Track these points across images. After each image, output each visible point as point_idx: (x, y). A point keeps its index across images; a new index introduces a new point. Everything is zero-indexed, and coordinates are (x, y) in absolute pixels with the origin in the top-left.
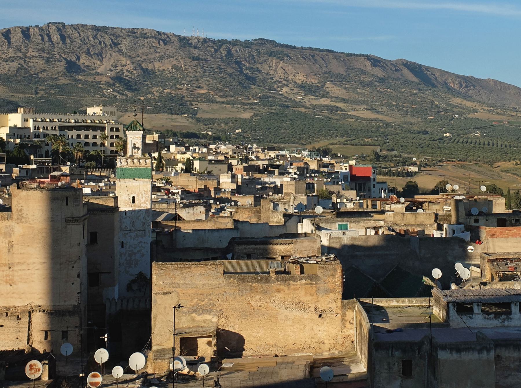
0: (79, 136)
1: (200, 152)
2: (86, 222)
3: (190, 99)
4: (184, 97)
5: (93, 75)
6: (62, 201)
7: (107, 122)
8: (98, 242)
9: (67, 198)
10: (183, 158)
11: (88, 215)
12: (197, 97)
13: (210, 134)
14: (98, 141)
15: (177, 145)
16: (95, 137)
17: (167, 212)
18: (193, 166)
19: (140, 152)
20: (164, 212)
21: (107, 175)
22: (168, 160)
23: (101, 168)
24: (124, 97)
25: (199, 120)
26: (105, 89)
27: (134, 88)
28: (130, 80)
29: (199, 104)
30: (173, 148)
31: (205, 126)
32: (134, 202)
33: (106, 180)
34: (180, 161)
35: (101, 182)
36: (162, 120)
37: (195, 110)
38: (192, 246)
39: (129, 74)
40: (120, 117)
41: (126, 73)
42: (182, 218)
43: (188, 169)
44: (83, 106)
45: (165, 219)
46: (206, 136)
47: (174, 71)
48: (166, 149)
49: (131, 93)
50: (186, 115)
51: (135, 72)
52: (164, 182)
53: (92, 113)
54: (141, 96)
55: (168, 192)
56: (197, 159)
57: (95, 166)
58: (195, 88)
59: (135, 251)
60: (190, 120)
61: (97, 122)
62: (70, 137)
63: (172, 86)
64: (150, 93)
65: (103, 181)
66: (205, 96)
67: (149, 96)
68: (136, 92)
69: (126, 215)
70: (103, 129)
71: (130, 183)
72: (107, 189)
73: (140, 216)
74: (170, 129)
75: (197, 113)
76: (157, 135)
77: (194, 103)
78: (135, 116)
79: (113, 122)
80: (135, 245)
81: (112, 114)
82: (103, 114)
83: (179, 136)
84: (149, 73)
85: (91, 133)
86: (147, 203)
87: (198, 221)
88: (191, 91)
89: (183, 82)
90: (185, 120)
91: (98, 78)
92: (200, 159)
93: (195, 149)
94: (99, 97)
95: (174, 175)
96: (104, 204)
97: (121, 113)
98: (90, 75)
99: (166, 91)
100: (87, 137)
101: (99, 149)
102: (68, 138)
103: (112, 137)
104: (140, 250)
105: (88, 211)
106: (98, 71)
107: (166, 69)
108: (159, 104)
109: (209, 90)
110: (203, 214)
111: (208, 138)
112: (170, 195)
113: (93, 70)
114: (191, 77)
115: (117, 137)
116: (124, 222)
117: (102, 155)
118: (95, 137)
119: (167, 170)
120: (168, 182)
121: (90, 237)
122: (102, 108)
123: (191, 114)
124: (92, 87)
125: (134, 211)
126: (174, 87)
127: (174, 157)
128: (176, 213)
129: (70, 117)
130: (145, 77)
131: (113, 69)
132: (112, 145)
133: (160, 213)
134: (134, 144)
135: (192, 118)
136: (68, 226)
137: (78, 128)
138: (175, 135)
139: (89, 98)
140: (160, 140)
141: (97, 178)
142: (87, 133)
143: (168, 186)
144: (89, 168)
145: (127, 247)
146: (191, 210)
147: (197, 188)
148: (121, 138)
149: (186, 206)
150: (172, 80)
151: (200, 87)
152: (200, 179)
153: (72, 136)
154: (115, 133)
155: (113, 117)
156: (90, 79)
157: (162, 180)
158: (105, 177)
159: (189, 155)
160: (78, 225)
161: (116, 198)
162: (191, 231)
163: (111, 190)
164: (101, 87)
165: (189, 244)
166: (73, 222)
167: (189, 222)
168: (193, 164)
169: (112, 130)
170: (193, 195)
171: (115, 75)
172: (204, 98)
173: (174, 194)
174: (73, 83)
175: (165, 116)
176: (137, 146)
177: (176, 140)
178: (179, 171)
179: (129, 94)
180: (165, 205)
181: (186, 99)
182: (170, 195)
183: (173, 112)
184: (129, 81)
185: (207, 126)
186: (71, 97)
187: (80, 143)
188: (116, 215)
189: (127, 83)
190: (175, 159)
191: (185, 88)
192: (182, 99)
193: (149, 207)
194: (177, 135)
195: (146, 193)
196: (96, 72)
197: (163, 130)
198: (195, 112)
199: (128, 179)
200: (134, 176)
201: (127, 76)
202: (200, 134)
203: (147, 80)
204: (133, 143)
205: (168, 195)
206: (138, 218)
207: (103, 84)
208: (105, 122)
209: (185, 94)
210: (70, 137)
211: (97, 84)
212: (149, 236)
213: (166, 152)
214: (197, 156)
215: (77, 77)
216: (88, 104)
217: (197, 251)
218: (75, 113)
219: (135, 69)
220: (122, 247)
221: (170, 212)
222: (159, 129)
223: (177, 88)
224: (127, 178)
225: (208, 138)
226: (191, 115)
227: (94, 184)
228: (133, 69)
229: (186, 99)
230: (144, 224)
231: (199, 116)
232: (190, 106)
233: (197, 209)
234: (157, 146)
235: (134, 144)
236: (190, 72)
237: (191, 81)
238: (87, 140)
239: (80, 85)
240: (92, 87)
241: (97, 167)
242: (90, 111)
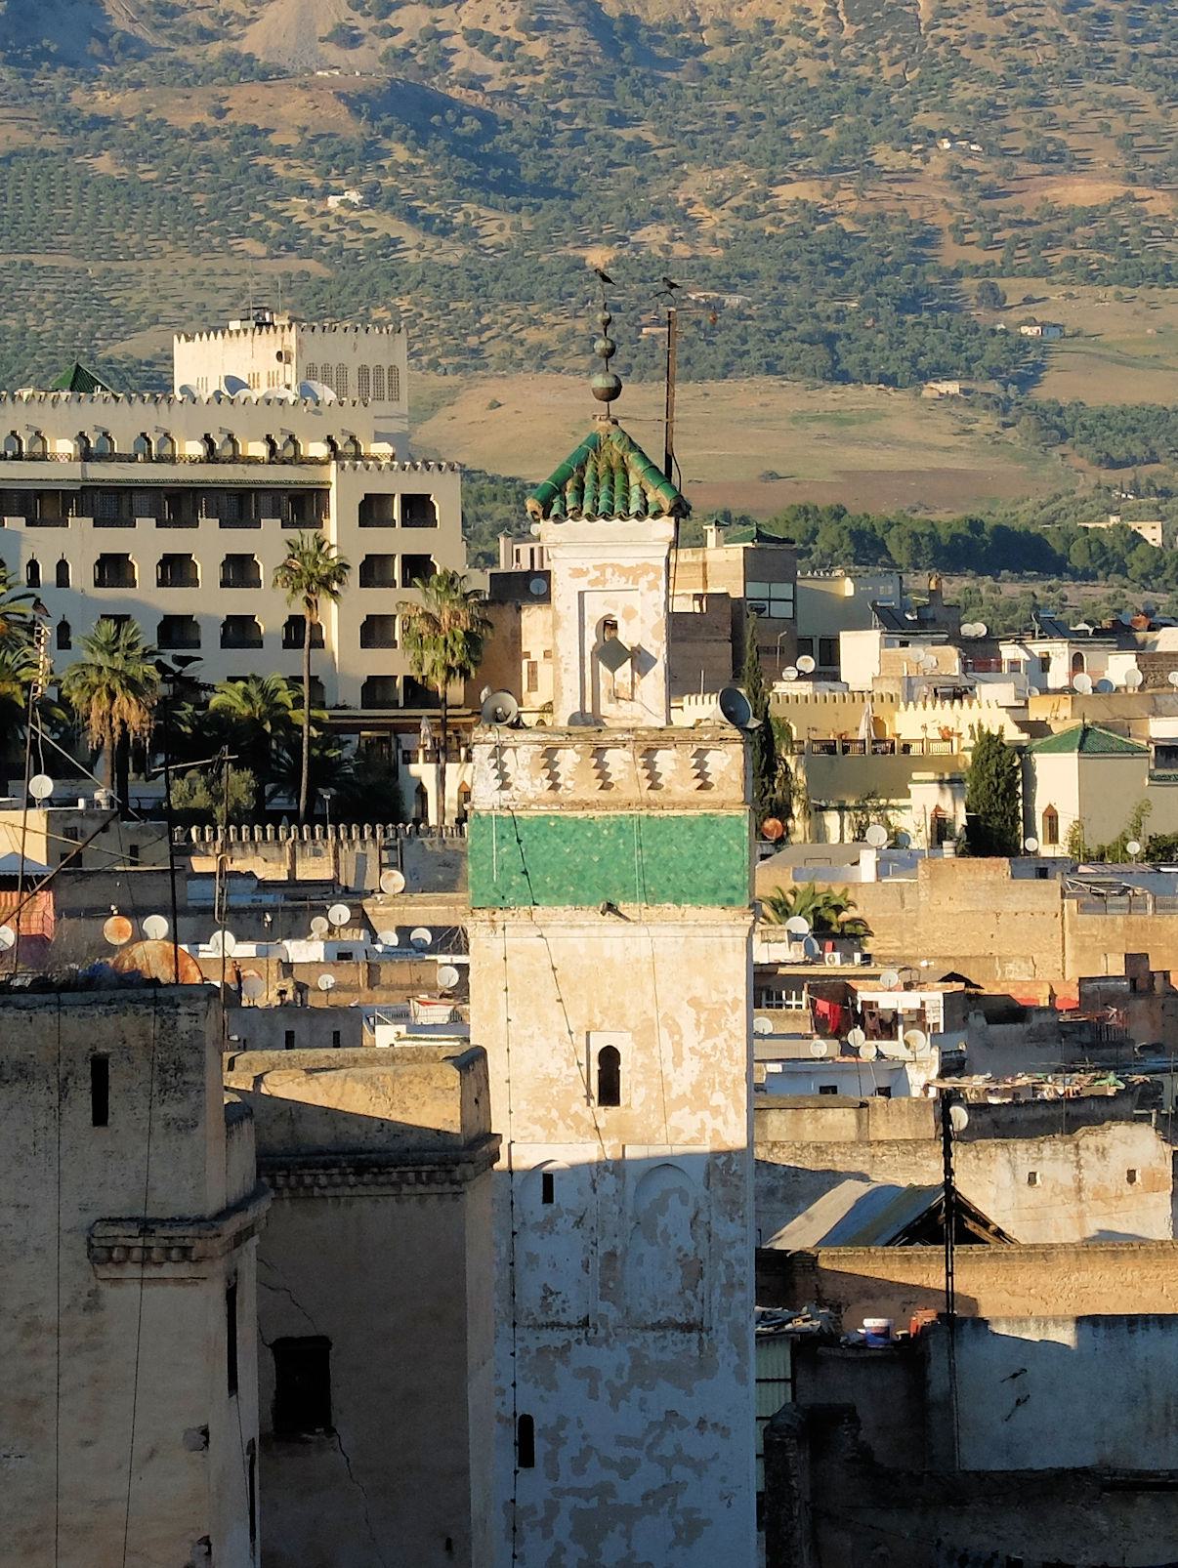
0: (113, 569)
1: (1084, 682)
2: (248, 1261)
3: (977, 256)
4: (929, 238)
5: (202, 76)
6: (63, 1090)
7: (335, 453)
8: (337, 1419)
9: (100, 1068)
10: (947, 736)
11: (265, 1205)
12: (1041, 243)
13: (1152, 533)
14: (269, 606)
15: (901, 624)
16: (239, 570)
17: (863, 1177)
18: (1029, 798)
19: (654, 683)
20: (831, 1179)
21: (348, 879)
22: (829, 748)
23: (294, 817)
24: (454, 253)
25: (1057, 427)
26: (304, 189)
27: (529, 174)
28: (502, 110)
29: (1056, 295)
30: (862, 653)
31: (1108, 476)
32: (609, 1093)
33: (341, 913)
34: (925, 762)
35: (303, 933)
36: (752, 429)
37: (1023, 344)
38: (1086, 1457)
39: (492, 67)
40: (425, 410)
41: (466, 59)
42: (985, 1223)
43: (994, 826)
44: (127, 323)
45: (850, 1232)
46: (1112, 558)
47: (848, 32)
48: (807, 663)
49: (508, 219)
50: (952, 387)
51: (538, 49)
52: (801, 925)
53: (216, 384)
54: (585, 243)
55: (841, 1012)
56: (1060, 745)
57: (247, 801)
58: (1024, 168)
59: (629, 1492)
60: (987, 422)
61: (259, 450)
62: (47, 574)
63: (839, 151)
64: (657, 216)
65: (319, 924)
66: (1102, 226)
67: (653, 236)
68: (552, 208)
69: (548, 1197)
70: (303, 505)
71: (575, 936)
72: (353, 989)
73: (661, 1206)
74: (825, 500)
75: (1039, 367)
76: (735, 553)
77: (1013, 288)
78: (613, 393)
79: (384, 449)
80: (622, 1441)
81: (376, 383)
82: (305, 391)
83: (900, 555)
84: (644, 57)
85: (208, 542)
86: (718, 1099)
87: (1111, 1245)
88: (989, 193)
89: (924, 119)
90: (947, 423)
91: (247, 103)
92: (1084, 741)
93: (1045, 663)
94: (258, 249)
95: (882, 871)
96: (380, 1110)
97: (435, 380)
98: (188, 77)
99: (786, 193)
100: (176, 570)
101: (274, 665)
102: (34, 580)
103: (374, 571)
104: (671, 1489)
105: (261, 1168)
106: (245, 47)
107: (784, 19)
108: (733, 300)
109: (1132, 179)
110: (1153, 1187)
111: (1137, 568)
112: (856, 1036)
113: (206, 36)
114: (987, 77)
115: (418, 567)
116: (533, 1259)
117: (299, 716)
118: (239, 570)
119: (819, 834)
120: (832, 928)
121: (272, 1375)
122: (291, 340)
123: (993, 373)
124: (203, 176)
125: (616, 1168)
126: (849, 163)
127: (877, 723)
128: (948, 1187)
129: (42, 416)
130: (621, 87)
131: (363, 24)
132: (375, 632)
133: (795, 1188)
134: (608, 625)
135: (1003, 406)
136: (110, 1293)
137: (110, 504)
138: (866, 547)
139: (172, 267)
140: (759, 590)
141: (268, 900)
142: (176, 540)
143: (834, 963)
144: (203, 818)
145: (564, 1456)
146: (1051, 1160)
147: (1073, 974)
148: (451, 581)
149: (1003, 1123)
150: (838, 106)
151: (1057, 159)
152: (1097, 899)
153: (62, 566)
154: (398, 541)
155: (384, 407)
156: (187, 113)
157: (783, 910)
158: (331, 890)
159: (991, 708)
160: (196, 1280)
161: (471, 1062)
162: (1065, 1336)
163: (381, 997)
164: (267, 177)
165: (1058, 1442)
166: (144, 1262)
167: (1042, 1253)
168: (1030, 781)
169: (372, 510)
170: (1038, 1038)
171: (383, 76)
172: (1100, 243)
173: (887, 1026)
174: (50, 142)
175: (788, 397)
176: (627, 637)
177: (887, 591)
178: (919, 842)
179: (497, 227)
180: (839, 1121)
181: (950, 254)
182: (856, 1036)
183: (850, 362)
184: (487, 118)
185: (1126, 475)
186: (40, 260)
187: (121, 620)
188: (479, 1203)
189: (477, 139)
190: (883, 746)
191: (937, 166)
192: (918, 260)
193: (735, 1136)
194: (881, 547)
195: (710, 1020)
196: (232, 59)
197: (772, 508)
198: (1022, 368)
199: (564, 912)
200: (606, 886)
201: (475, 83)
202: (1069, 540)
203: (636, 107)
204: (595, 612)
205: (839, 1033)
206: (644, 1225)
207: (283, 151)
208: (320, 450)
209: (943, 220)
210: (47, 574)
211: (237, 150)
212: (741, 1376)
213: (806, 688)
214: (1062, 717)
215: (78, 97)
216: (168, 310)
217: (1143, 1501)
218: (81, 382)
219: (541, 26)
220: (526, 1458)
221: (881, 1177)
222: (737, 508)
223: (871, 171)
224: (558, 896)
225: (1137, 568)
226: (993, 387)
227: (248, 949)
228: (524, 26)
229: (950, 254)
230: (694, 1272)
231: (1052, 389)
232: (981, 315)
233: (1102, 1152)
234: (736, 638)
235: (608, 625)
236: (978, 41)
237: (990, 111)
238: (176, 601)
239: (104, 164)
240: (203, 176)
241: (260, 814)
242: (199, 363)
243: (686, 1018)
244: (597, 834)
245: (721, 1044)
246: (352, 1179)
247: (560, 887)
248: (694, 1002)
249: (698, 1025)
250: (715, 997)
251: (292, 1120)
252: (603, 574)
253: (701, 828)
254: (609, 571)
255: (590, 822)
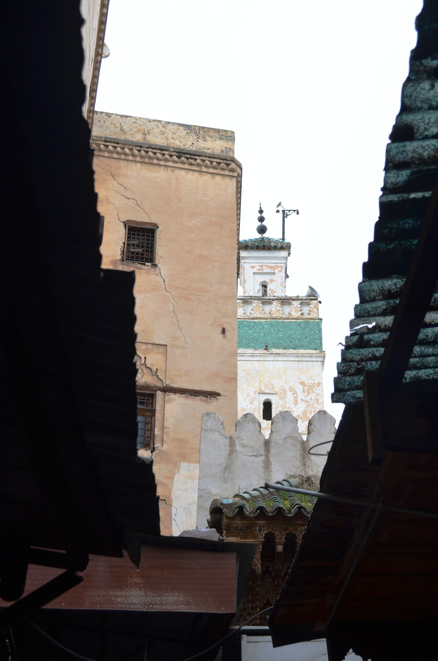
8: (158, 260)
243: (299, 389)
244: (263, 328)
245: (313, 397)
246: (175, 158)
247: (249, 343)
248: (302, 383)
249: (304, 391)
250: (310, 381)
251: (144, 134)
252: (262, 267)
253: (303, 326)
254: (264, 267)
255: (260, 323)
